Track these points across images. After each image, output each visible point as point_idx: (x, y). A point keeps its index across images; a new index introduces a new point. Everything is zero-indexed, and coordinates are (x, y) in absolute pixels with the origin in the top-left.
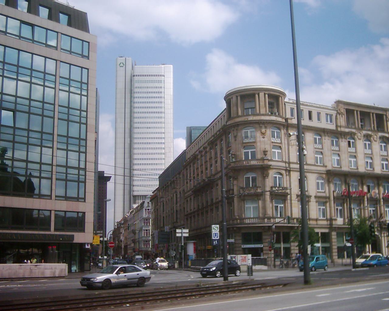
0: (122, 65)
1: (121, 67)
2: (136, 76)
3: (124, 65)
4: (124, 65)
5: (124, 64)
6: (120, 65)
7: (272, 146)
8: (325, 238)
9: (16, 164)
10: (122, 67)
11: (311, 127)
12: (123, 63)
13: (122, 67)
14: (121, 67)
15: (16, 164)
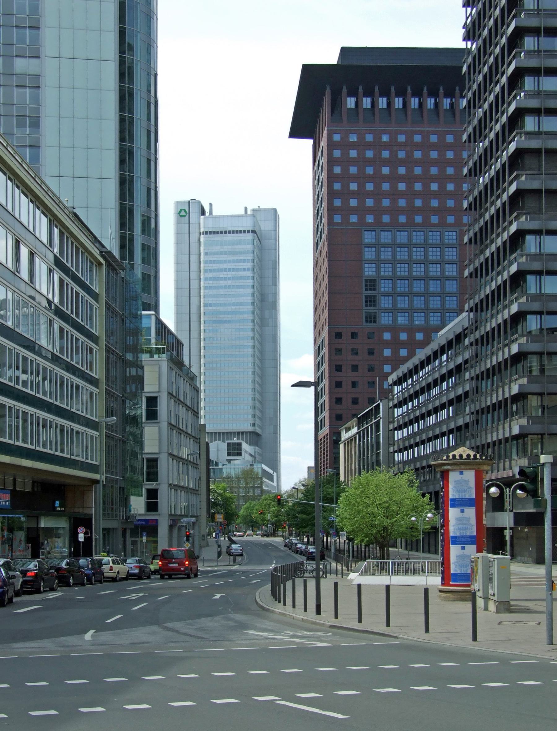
0: (183, 213)
1: (181, 216)
5: (188, 212)
10: (184, 216)
12: (185, 210)
13: (184, 216)
14: (181, 216)
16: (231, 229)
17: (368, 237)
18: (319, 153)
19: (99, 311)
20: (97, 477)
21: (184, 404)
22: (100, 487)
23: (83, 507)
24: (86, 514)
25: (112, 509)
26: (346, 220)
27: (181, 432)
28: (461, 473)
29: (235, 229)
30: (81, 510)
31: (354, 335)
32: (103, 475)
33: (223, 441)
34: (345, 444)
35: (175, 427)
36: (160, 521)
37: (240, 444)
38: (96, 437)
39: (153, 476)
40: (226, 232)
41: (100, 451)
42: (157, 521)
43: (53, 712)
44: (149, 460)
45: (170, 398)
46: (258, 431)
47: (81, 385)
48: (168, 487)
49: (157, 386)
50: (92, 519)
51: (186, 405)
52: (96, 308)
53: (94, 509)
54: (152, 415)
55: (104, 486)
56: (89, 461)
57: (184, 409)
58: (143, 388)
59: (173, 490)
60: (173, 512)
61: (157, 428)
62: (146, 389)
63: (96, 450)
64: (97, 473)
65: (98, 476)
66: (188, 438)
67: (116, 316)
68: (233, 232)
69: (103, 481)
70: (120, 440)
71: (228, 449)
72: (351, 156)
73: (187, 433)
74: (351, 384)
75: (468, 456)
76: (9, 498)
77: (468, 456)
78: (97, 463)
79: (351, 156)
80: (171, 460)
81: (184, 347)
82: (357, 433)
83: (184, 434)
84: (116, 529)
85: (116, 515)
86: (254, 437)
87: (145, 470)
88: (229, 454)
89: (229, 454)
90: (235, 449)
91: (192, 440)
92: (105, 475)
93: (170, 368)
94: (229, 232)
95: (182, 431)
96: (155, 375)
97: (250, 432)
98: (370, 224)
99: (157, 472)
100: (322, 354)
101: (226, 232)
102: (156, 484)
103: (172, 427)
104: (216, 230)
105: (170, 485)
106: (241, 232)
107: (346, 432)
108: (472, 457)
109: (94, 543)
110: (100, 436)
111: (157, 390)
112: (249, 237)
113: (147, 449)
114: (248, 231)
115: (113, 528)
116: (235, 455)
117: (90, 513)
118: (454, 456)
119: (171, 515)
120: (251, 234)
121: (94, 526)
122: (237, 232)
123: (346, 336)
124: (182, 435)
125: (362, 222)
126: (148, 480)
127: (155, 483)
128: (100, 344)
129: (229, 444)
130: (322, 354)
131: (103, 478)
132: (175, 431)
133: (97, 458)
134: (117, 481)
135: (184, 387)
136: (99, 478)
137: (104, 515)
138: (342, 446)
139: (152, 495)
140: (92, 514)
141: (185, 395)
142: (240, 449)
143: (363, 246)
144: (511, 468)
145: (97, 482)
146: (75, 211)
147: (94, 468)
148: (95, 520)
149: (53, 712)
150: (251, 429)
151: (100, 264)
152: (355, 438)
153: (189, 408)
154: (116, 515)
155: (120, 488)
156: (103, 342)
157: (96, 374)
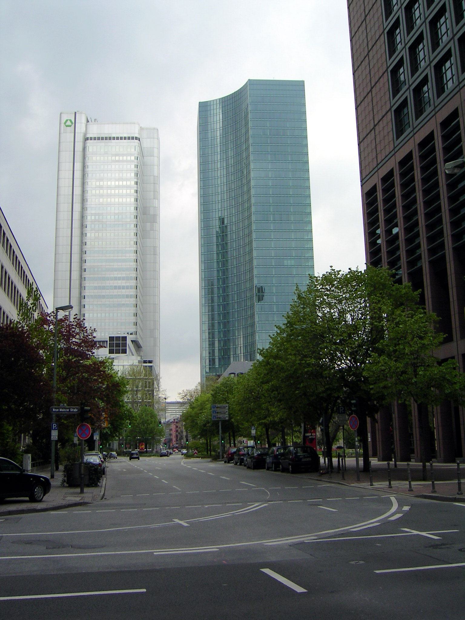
0: (69, 123)
1: (67, 126)
2: (91, 139)
3: (72, 123)
4: (72, 123)
5: (73, 122)
6: (65, 123)
7: (153, 362)
8: (326, 378)
9: (210, 149)
10: (70, 126)
11: (30, 513)
12: (71, 120)
13: (70, 126)
14: (67, 126)
15: (210, 149)
16: (115, 136)
28: (82, 492)
29: (120, 136)
40: (110, 138)
43: (377, 572)
68: (118, 138)
76: (52, 437)
90: (118, 345)
94: (114, 138)
101: (110, 138)
106: (125, 138)
116: (118, 352)
122: (121, 138)
144: (235, 446)
149: (377, 572)
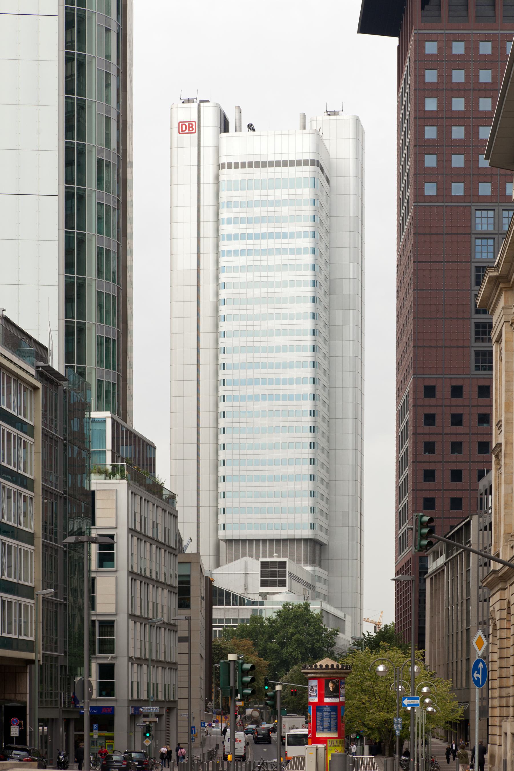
16: (274, 158)
17: (483, 221)
18: (406, 69)
19: (35, 447)
20: (31, 656)
21: (153, 540)
22: (36, 668)
23: (16, 693)
24: (19, 702)
25: (51, 694)
26: (444, 190)
27: (147, 581)
30: (13, 696)
31: (457, 391)
32: (40, 653)
33: (257, 558)
34: (431, 579)
35: (140, 575)
36: (116, 708)
37: (283, 565)
38: (31, 607)
39: (108, 646)
41: (36, 622)
42: (113, 708)
44: (102, 624)
45: (132, 536)
46: (323, 537)
47: (13, 545)
48: (128, 661)
49: (114, 519)
50: (26, 707)
51: (157, 541)
52: (31, 445)
53: (28, 695)
54: (107, 555)
55: (41, 667)
56: (22, 637)
57: (154, 547)
58: (94, 524)
59: (135, 665)
60: (135, 697)
61: (114, 579)
62: (99, 523)
63: (31, 622)
64: (32, 651)
65: (34, 654)
66: (160, 589)
67: (56, 442)
69: (39, 661)
70: (61, 604)
71: (263, 574)
72: (454, 80)
73: (157, 581)
74: (450, 474)
75: (332, 666)
77: (332, 666)
78: (32, 639)
79: (454, 80)
80: (132, 623)
81: (157, 451)
82: (445, 564)
83: (154, 583)
84: (56, 719)
85: (56, 701)
86: (316, 549)
87: (97, 637)
88: (264, 583)
89: (264, 583)
91: (166, 591)
92: (41, 652)
93: (132, 493)
94: (271, 164)
95: (150, 579)
96: (113, 501)
97: (306, 540)
98: (485, 199)
99: (113, 641)
100: (405, 420)
102: (112, 657)
103: (135, 577)
104: (246, 160)
105: (130, 658)
106: (292, 163)
107: (434, 560)
108: (335, 667)
109: (28, 737)
110: (36, 604)
111: (114, 525)
112: (308, 172)
113: (100, 608)
114: (306, 163)
115: (53, 719)
116: (273, 584)
117: (24, 699)
118: (321, 666)
119: (133, 700)
120: (310, 168)
121: (28, 716)
123: (444, 392)
124: (151, 586)
125: (471, 192)
126: (101, 652)
127: (110, 655)
128: (35, 490)
129: (264, 565)
130: (405, 420)
131: (40, 657)
132: (138, 582)
133: (32, 632)
134: (56, 658)
135: (153, 515)
136: (34, 658)
137: (41, 702)
138: (428, 581)
139: (107, 672)
140: (26, 702)
141: (155, 525)
142: (284, 574)
143: (474, 236)
145: (32, 662)
146: (5, 313)
147: (29, 646)
148: (30, 709)
150: (307, 533)
151: (36, 388)
152: (443, 571)
153: (160, 545)
154: (56, 701)
155: (61, 666)
156: (39, 541)
157: (31, 420)
